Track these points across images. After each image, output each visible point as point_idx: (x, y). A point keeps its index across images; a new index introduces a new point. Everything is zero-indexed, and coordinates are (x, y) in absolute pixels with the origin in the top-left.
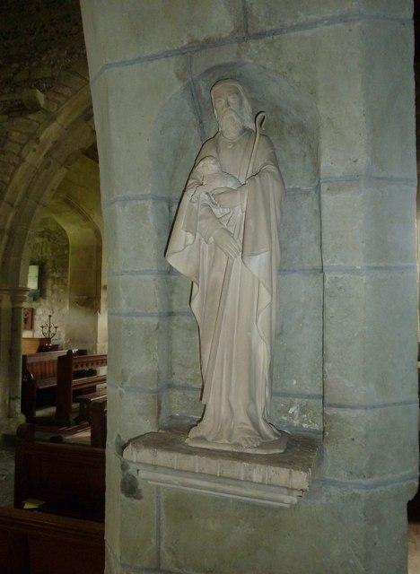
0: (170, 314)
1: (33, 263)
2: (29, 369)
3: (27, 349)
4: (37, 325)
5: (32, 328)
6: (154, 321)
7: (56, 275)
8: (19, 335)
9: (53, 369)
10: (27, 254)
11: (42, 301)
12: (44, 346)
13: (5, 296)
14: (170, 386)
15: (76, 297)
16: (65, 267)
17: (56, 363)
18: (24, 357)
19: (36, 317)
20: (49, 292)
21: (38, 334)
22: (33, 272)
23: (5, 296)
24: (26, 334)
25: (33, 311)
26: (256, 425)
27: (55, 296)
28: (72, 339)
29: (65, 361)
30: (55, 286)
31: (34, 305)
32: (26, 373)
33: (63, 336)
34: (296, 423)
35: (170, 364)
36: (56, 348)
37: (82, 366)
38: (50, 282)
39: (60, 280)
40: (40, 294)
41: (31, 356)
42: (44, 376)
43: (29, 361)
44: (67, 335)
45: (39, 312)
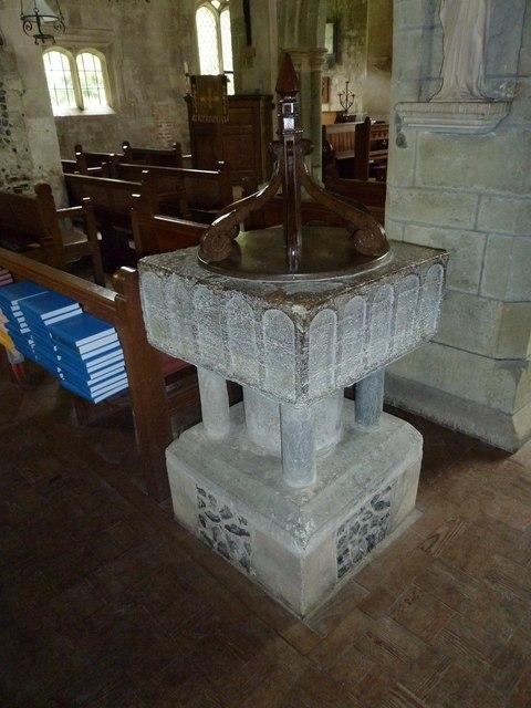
0: (432, 28)
1: (328, 21)
2: (328, 139)
3: (325, 120)
4: (334, 97)
5: (328, 100)
6: (420, 32)
7: (353, 33)
8: (319, 107)
9: (350, 141)
10: (321, 18)
11: (338, 67)
12: (341, 118)
13: (304, 59)
14: (429, 79)
15: (375, 59)
16: (362, 19)
17: (353, 135)
18: (324, 127)
19: (332, 87)
20: (345, 56)
21: (336, 106)
22: (329, 30)
23: (304, 59)
24: (324, 108)
25: (328, 81)
26: (471, 89)
27: (352, 60)
28: (369, 108)
29: (364, 129)
30: (352, 48)
31: (330, 73)
32: (326, 144)
33: (360, 107)
34: (503, 94)
35: (430, 65)
36: (353, 118)
37: (380, 135)
38: (346, 42)
39: (357, 40)
40: (336, 59)
41: (330, 126)
42: (342, 148)
43: (328, 131)
44: (364, 108)
45: (335, 81)
